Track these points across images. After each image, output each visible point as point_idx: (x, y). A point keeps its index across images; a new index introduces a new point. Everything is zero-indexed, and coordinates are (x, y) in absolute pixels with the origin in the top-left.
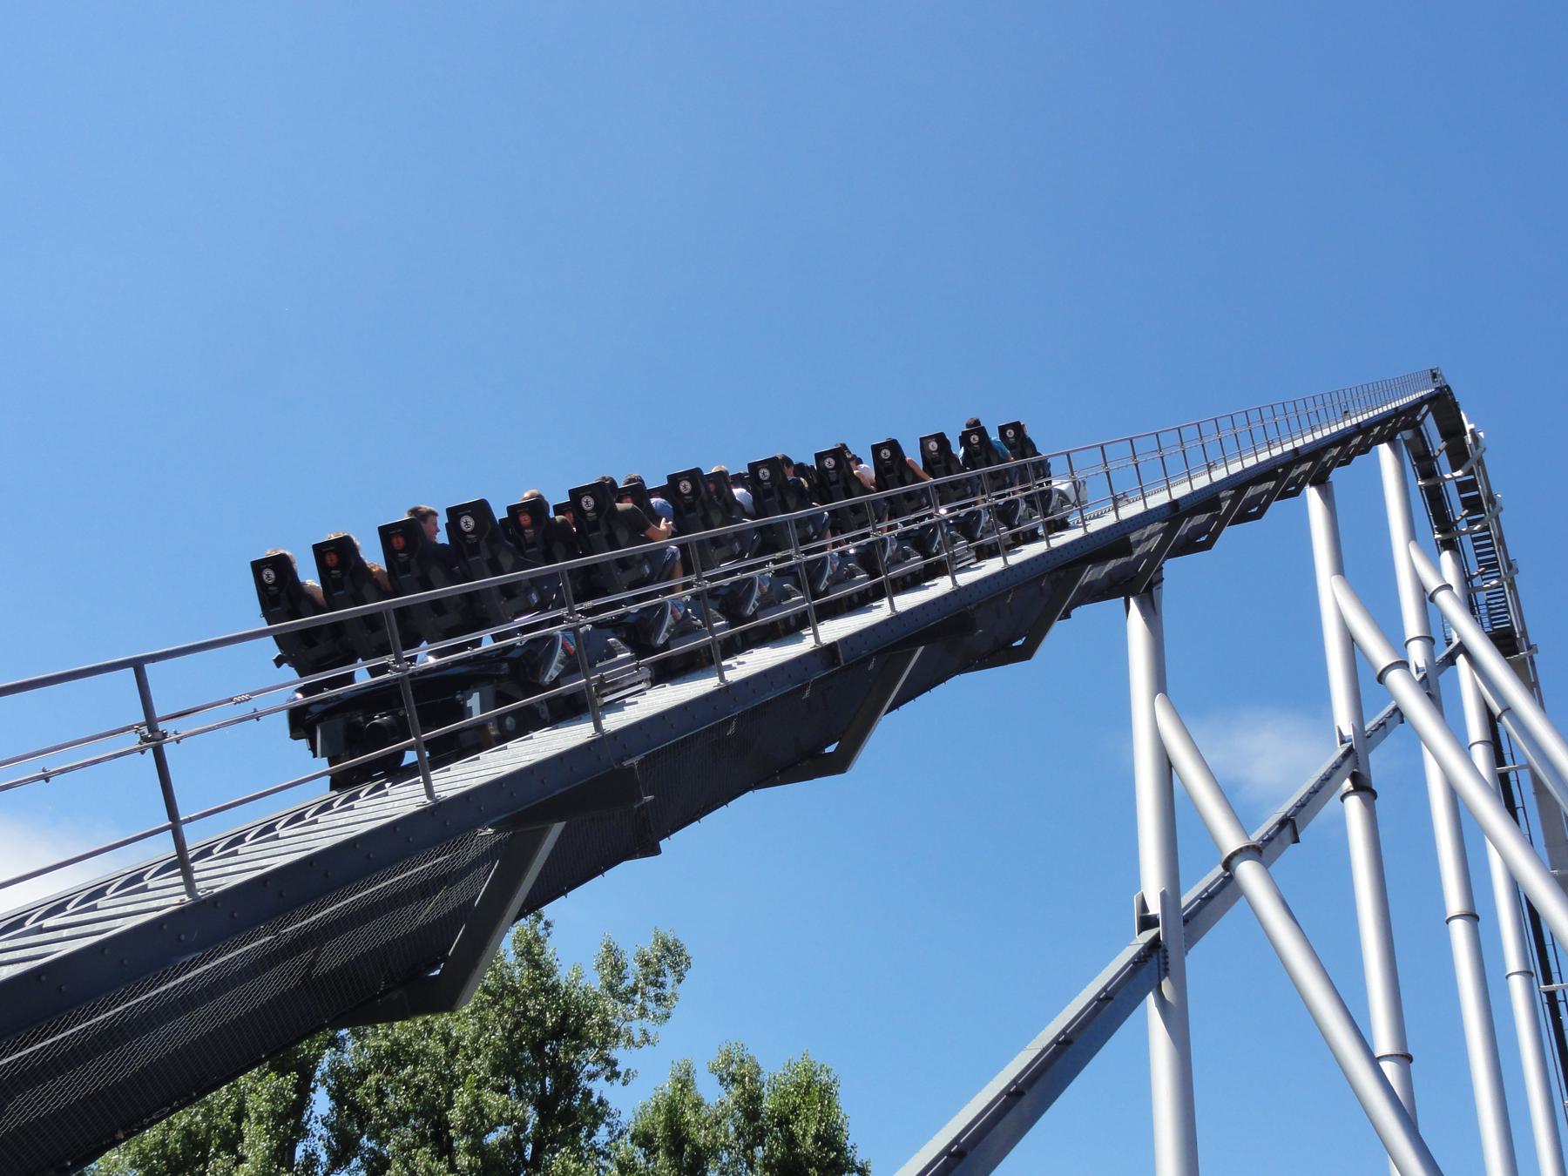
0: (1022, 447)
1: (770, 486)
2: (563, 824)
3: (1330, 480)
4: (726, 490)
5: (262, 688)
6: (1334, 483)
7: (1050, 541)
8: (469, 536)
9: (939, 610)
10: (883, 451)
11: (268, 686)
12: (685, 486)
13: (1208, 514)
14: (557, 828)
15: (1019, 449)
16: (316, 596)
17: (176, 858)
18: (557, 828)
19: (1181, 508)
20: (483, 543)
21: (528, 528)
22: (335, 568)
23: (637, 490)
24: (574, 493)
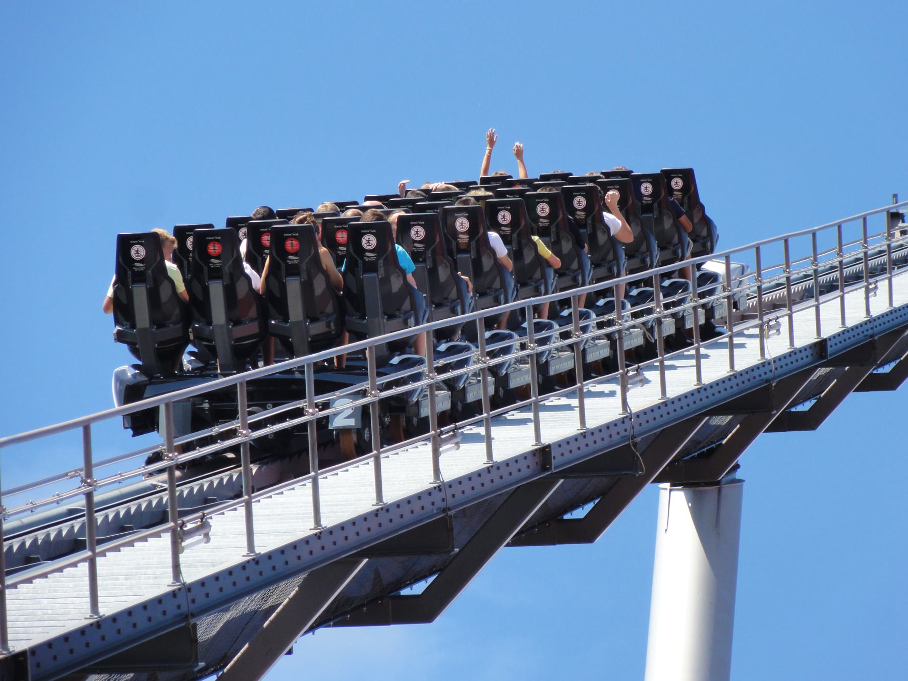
0: (519, 243)
1: (583, 217)
2: (367, 559)
3: (739, 475)
4: (482, 231)
5: (805, 235)
6: (746, 486)
7: (667, 372)
8: (136, 264)
9: (193, 601)
10: (541, 205)
11: (774, 243)
12: (137, 252)
13: (831, 368)
14: (366, 560)
15: (429, 265)
16: (431, 261)
17: (9, 581)
18: (366, 560)
19: (554, 462)
20: (656, 205)
21: (342, 245)
22: (295, 254)
23: (152, 241)
24: (232, 222)
